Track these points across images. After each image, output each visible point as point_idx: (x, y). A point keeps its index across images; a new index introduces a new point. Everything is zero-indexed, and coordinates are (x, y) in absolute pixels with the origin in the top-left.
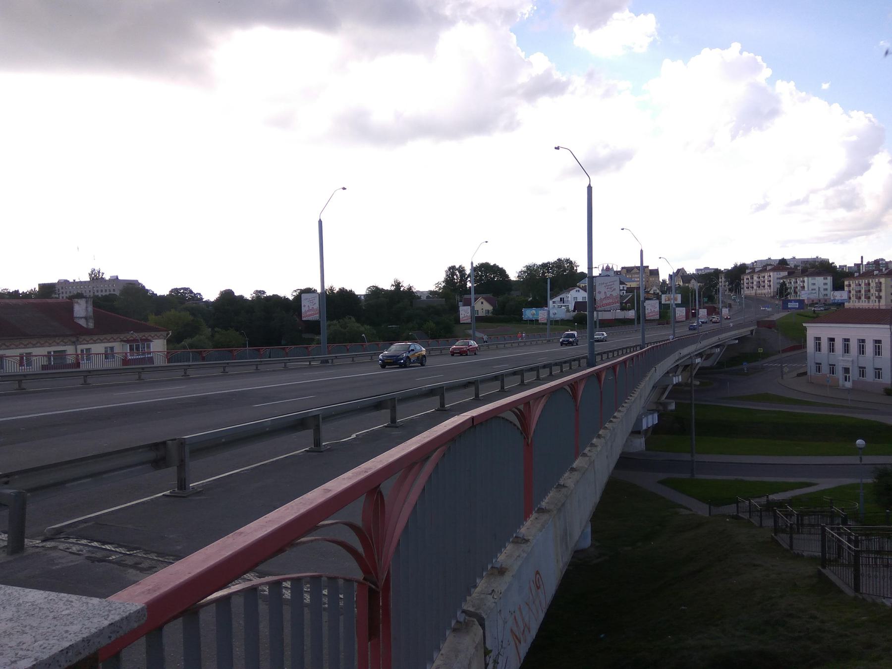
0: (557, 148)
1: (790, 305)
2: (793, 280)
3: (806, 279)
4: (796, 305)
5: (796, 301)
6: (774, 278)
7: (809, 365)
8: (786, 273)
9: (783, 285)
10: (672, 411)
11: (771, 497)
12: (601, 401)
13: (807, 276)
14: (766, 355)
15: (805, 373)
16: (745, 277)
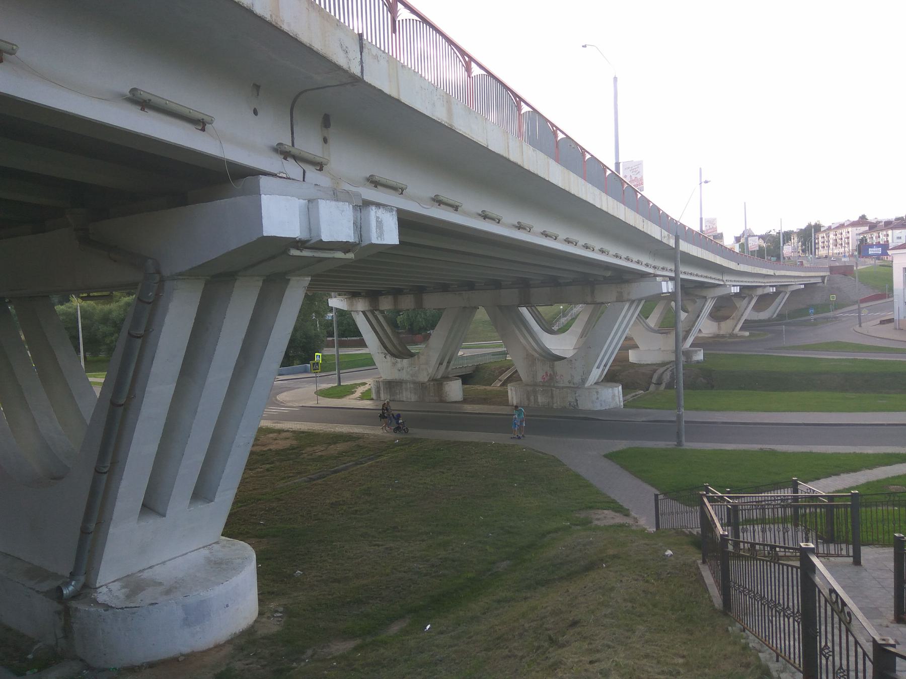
0: (585, 46)
1: (871, 251)
2: (875, 235)
3: (890, 232)
4: (879, 251)
5: (878, 245)
6: (853, 234)
7: (896, 306)
8: (867, 228)
9: (863, 241)
10: (698, 362)
11: (805, 488)
12: (318, 89)
13: (892, 229)
14: (838, 306)
15: (891, 321)
16: (821, 235)
